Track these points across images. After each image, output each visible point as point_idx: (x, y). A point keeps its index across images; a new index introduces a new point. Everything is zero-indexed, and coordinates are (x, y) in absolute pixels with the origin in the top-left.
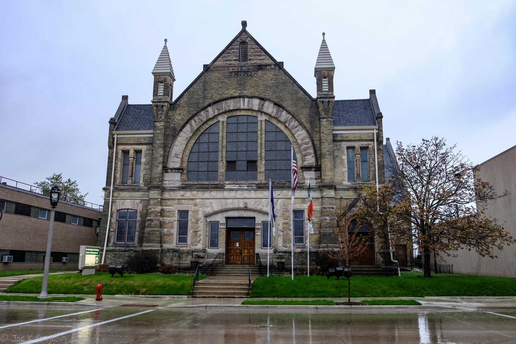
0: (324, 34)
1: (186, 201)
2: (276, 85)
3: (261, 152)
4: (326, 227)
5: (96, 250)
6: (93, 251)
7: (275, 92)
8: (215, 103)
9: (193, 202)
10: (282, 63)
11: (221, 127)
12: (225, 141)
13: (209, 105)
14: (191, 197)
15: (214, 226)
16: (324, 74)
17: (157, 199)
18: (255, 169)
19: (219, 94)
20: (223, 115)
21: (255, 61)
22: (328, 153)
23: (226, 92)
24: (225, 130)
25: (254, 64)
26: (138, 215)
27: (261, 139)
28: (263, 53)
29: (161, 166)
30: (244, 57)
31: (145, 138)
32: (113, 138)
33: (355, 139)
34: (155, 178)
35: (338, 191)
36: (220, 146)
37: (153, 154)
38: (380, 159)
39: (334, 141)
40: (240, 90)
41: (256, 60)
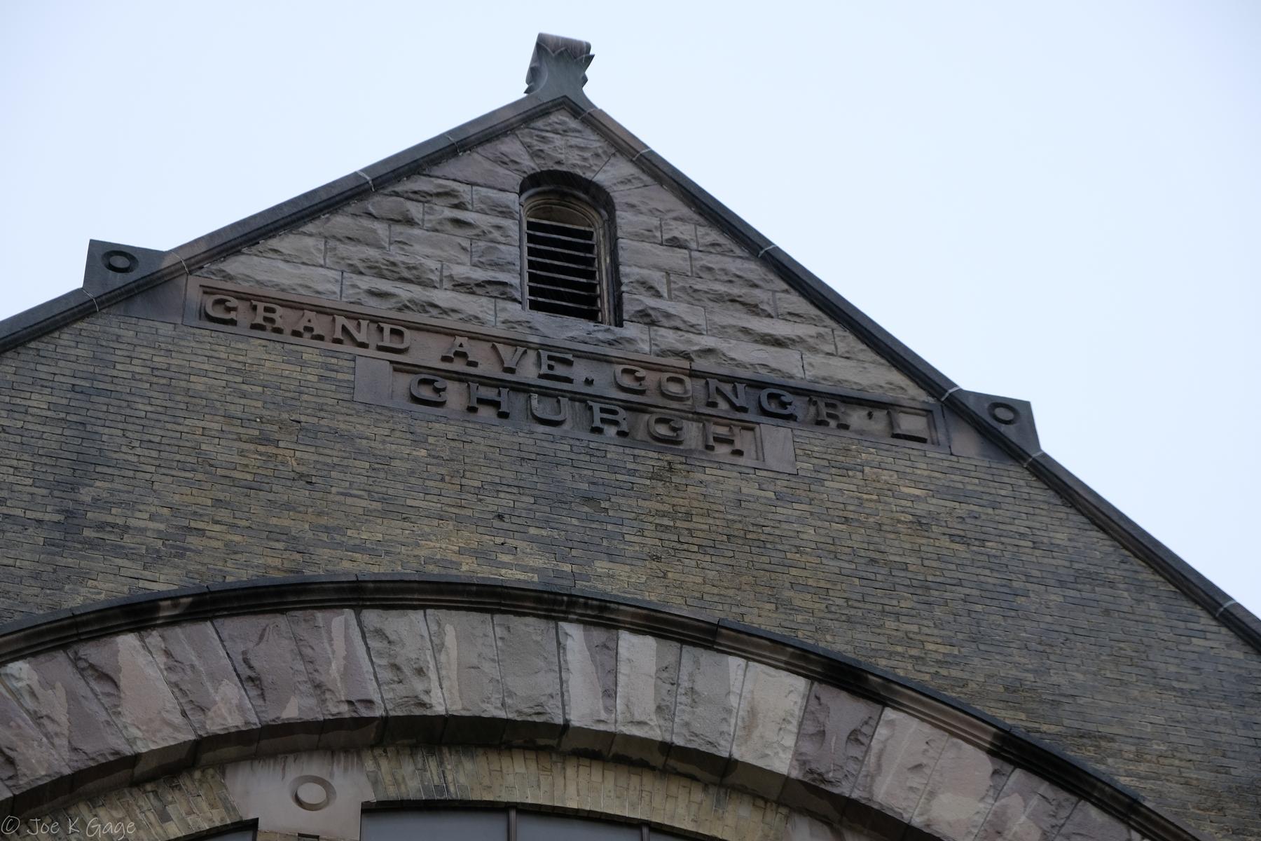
8: (208, 605)
13: (138, 615)
21: (708, 341)
25: (701, 364)
40: (546, 545)
41: (722, 331)
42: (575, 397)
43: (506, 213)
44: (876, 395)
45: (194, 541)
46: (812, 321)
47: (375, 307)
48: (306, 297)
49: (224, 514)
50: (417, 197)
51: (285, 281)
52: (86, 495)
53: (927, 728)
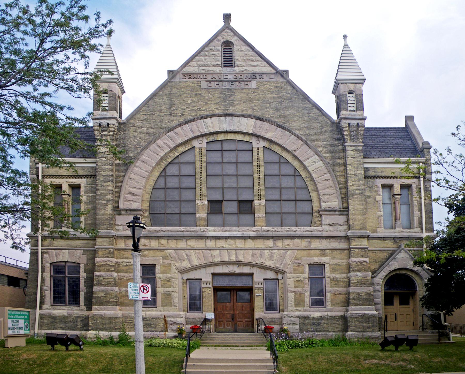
0: (345, 37)
1: (151, 252)
2: (279, 100)
3: (260, 188)
4: (357, 286)
5: (24, 313)
6: (19, 315)
7: (277, 110)
9: (163, 253)
10: (287, 72)
11: (197, 154)
12: (204, 175)
14: (158, 248)
15: (193, 284)
16: (348, 91)
17: (108, 248)
18: (252, 212)
19: (193, 110)
20: (201, 139)
22: (357, 192)
23: (203, 108)
24: (204, 160)
25: (245, 72)
26: (82, 270)
27: (260, 172)
28: (258, 58)
29: (110, 207)
30: (228, 61)
31: (84, 169)
32: (37, 169)
33: (393, 175)
34: (103, 221)
35: (371, 241)
36: (198, 181)
37: (96, 190)
38: (427, 202)
39: (366, 177)
40: (224, 106)
42: (228, 81)
43: (218, 51)
44: (268, 72)
45: (184, 113)
46: (260, 61)
47: (203, 72)
48: (194, 72)
49: (187, 109)
50: (207, 51)
51: (191, 70)
52: (172, 109)
53: (269, 124)
